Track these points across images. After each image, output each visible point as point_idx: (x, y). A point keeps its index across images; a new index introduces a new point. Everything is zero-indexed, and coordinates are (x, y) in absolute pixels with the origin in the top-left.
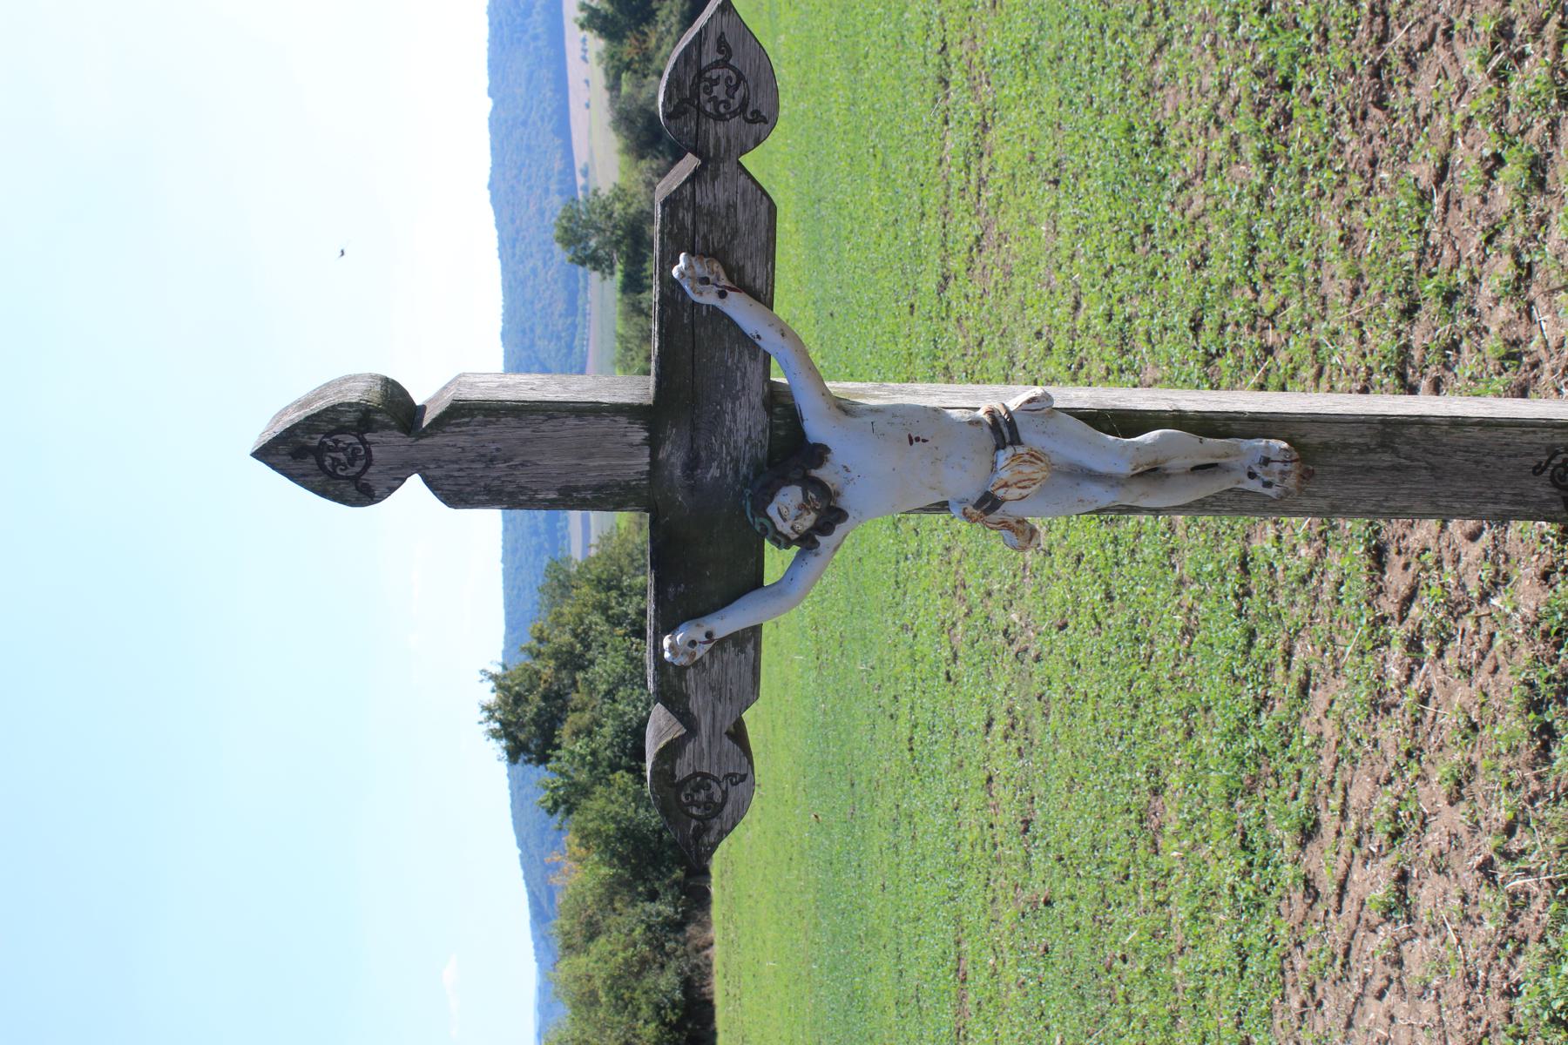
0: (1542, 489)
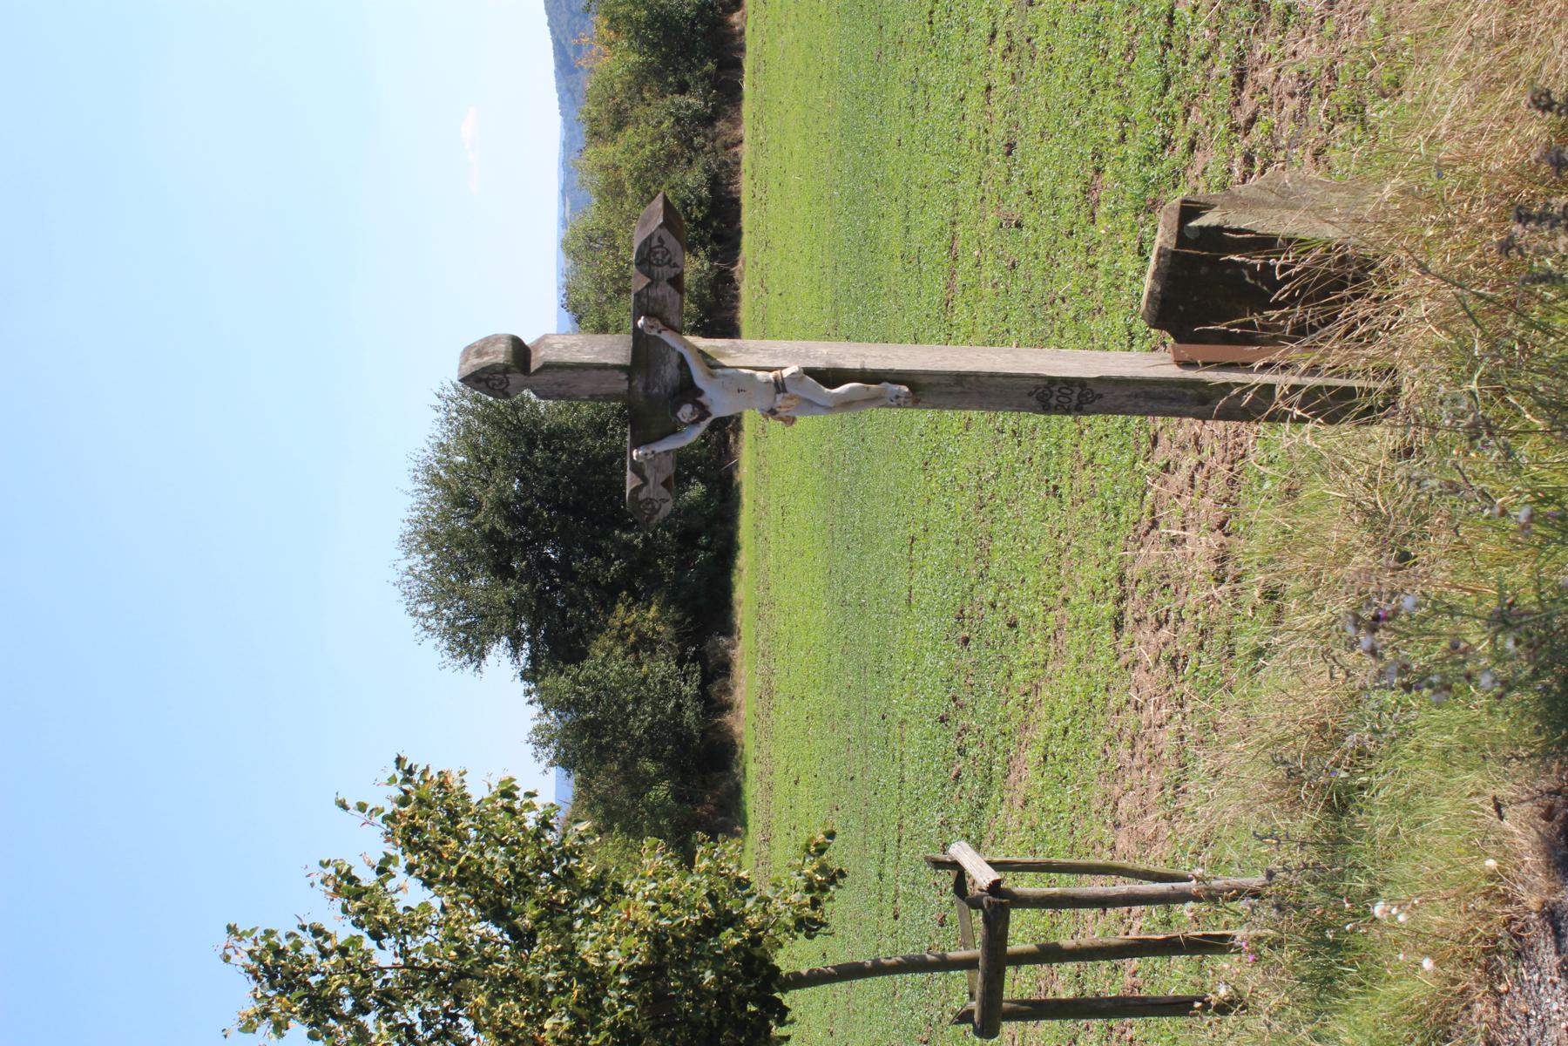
0: (1033, 401)
